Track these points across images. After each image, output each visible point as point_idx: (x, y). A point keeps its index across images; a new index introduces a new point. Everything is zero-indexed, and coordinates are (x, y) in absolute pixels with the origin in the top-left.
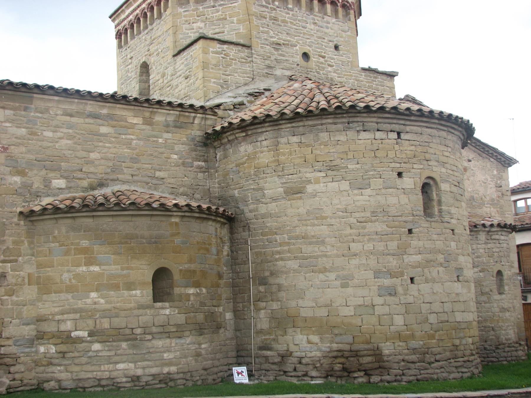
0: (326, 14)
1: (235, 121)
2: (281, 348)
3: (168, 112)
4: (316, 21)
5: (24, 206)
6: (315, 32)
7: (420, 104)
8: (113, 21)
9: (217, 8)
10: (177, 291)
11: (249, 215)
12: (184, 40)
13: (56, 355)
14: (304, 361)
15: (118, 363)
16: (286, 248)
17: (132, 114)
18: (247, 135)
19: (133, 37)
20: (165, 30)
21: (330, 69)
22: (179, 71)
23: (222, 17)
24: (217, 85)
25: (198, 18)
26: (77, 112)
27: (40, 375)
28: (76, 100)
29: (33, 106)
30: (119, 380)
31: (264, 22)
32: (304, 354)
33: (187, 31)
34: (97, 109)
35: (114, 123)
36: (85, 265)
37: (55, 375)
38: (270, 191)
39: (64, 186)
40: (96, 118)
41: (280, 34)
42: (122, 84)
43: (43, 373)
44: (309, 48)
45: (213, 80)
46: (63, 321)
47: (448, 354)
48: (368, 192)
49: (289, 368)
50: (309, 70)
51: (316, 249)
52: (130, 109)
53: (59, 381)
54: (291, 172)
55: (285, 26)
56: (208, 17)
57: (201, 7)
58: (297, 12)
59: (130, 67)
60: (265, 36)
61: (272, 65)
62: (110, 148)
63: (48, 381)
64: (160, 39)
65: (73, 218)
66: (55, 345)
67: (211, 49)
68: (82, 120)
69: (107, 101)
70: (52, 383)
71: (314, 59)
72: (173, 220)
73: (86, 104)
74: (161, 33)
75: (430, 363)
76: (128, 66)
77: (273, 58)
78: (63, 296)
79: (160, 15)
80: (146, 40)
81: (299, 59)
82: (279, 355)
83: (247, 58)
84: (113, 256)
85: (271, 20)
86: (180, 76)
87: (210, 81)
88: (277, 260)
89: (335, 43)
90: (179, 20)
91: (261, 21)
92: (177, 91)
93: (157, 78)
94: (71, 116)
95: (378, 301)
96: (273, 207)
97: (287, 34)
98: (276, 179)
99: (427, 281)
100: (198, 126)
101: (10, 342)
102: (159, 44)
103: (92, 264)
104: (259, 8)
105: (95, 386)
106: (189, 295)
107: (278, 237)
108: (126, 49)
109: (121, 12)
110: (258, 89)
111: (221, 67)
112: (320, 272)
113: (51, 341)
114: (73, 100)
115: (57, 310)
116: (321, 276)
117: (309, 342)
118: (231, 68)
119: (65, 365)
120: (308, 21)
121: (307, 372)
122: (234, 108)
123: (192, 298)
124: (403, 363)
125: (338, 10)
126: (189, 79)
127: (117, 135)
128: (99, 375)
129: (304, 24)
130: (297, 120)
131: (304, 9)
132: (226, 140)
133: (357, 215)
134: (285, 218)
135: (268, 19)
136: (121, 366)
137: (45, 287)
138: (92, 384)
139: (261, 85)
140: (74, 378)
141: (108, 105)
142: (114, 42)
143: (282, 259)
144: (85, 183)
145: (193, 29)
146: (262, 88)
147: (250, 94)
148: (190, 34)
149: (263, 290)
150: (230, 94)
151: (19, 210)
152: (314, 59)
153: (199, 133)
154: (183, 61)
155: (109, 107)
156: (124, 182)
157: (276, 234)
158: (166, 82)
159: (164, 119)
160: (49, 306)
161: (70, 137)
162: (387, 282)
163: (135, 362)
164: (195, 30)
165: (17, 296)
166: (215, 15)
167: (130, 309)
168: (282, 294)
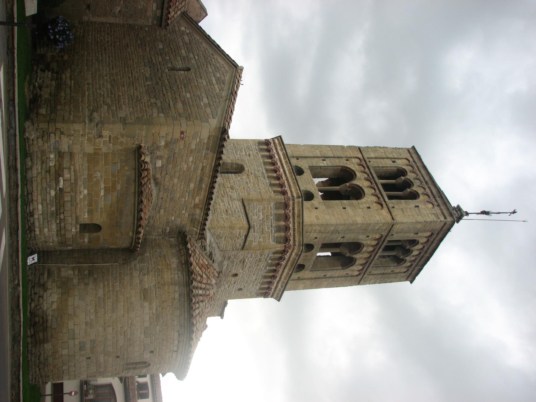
0: (262, 284)
1: (192, 259)
2: (49, 284)
5: (145, 147)
10: (87, 235)
11: (133, 263)
13: (48, 166)
14: (41, 299)
15: (42, 205)
16: (111, 289)
17: (201, 198)
18: (182, 264)
19: (263, 156)
21: (227, 286)
27: (35, 155)
29: (209, 152)
30: (31, 205)
32: (45, 299)
35: (196, 190)
36: (105, 187)
37: (35, 166)
38: (146, 279)
39: (157, 166)
42: (234, 144)
43: (37, 156)
46: (70, 171)
47: (44, 374)
48: (143, 336)
49: (37, 290)
51: (109, 308)
53: (31, 168)
54: (157, 293)
60: (249, 256)
62: (180, 188)
63: (31, 160)
66: (55, 166)
70: (30, 163)
71: (233, 279)
72: (131, 234)
74: (260, 187)
75: (38, 366)
77: (235, 259)
78: (86, 172)
79: (272, 185)
81: (234, 272)
82: (45, 283)
84: (110, 203)
88: (104, 282)
92: (220, 201)
93: (231, 182)
94: (202, 170)
95: (77, 342)
96: (137, 281)
98: (153, 284)
99: (88, 365)
100: (192, 230)
101: (57, 139)
103: (105, 191)
105: (28, 191)
106: (84, 239)
107: (118, 284)
112: (96, 310)
113: (57, 163)
115: (77, 168)
116: (93, 310)
117: (53, 302)
119: (41, 173)
121: (34, 301)
123: (82, 240)
124: (38, 354)
127: (188, 190)
128: (35, 194)
129: (256, 274)
131: (266, 274)
132: (181, 248)
133: (129, 331)
136: (40, 207)
137: (93, 159)
138: (29, 190)
139: (218, 256)
140: (33, 179)
141: (208, 189)
143: (104, 286)
144: (158, 176)
147: (211, 254)
149: (85, 273)
150: (212, 240)
151: (143, 145)
153: (187, 229)
156: (158, 195)
157: (120, 283)
160: (80, 162)
161: (188, 168)
162: (88, 346)
163: (42, 214)
165: (87, 143)
167: (76, 212)
168: (82, 286)
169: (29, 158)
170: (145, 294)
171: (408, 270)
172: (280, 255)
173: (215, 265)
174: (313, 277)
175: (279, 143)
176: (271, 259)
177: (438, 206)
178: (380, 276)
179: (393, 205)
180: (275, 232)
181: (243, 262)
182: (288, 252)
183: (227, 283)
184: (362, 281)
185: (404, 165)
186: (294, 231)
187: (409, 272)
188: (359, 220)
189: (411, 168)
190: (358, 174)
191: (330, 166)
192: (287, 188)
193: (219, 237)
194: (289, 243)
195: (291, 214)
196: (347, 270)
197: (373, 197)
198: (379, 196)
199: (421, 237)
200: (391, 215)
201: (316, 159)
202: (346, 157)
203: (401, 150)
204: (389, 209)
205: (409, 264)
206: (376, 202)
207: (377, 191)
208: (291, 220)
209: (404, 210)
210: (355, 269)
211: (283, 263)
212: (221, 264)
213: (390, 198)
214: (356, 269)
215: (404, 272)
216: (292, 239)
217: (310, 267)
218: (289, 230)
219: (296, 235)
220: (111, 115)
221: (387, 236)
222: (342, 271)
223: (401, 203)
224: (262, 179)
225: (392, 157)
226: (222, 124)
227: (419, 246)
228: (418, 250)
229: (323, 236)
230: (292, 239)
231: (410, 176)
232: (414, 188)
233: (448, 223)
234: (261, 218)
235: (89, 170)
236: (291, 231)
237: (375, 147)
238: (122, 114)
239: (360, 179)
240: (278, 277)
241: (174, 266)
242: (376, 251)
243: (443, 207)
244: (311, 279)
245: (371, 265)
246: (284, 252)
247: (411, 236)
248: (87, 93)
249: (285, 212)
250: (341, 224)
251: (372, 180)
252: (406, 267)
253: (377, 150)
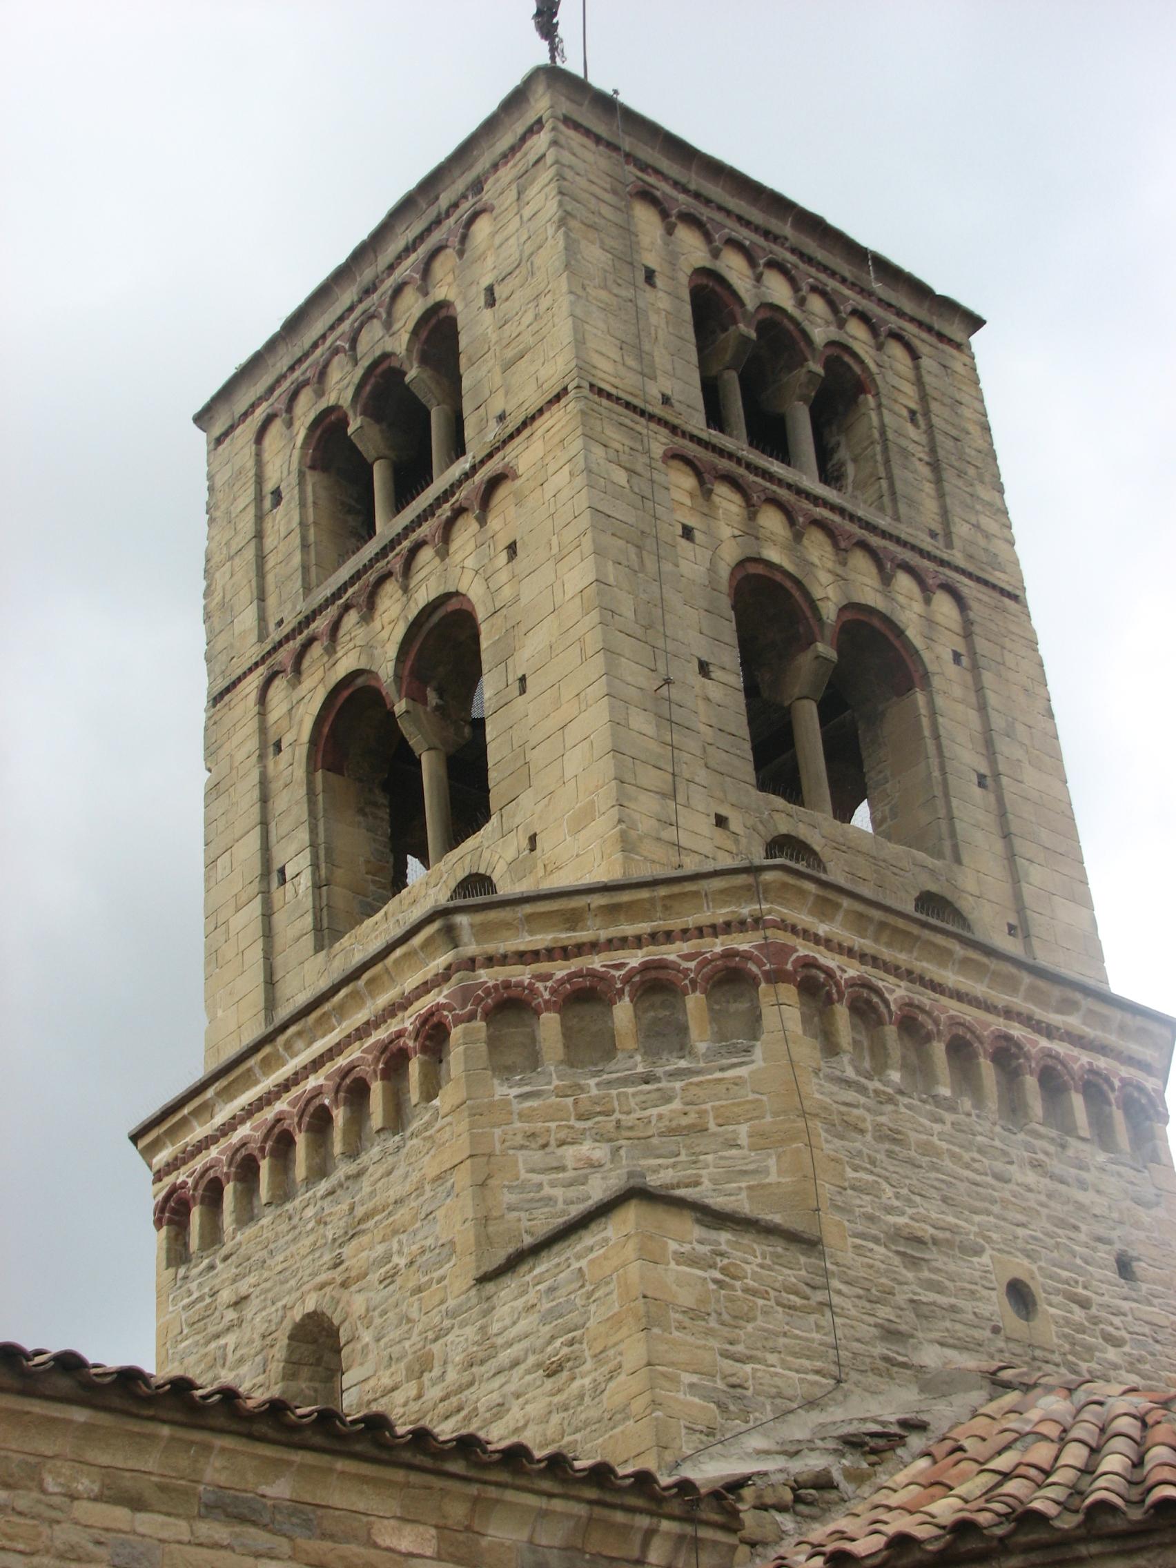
0: (1069, 1129)
3: (542, 1503)
4: (1041, 1156)
6: (1043, 1198)
8: (148, 1153)
9: (663, 1084)
12: (523, 1215)
19: (247, 1216)
20: (432, 1172)
21: (1112, 1354)
22: (509, 1344)
23: (685, 1121)
24: (704, 1397)
25: (580, 1125)
26: (162, 1488)
28: (166, 1431)
31: (858, 1145)
33: (536, 1178)
34: (250, 1476)
40: (242, 1519)
41: (918, 1199)
44: (1026, 1262)
45: (687, 1378)
50: (1038, 1353)
52: (391, 1484)
55: (934, 1168)
56: (628, 1120)
57: (592, 1082)
58: (969, 1115)
59: (230, 1340)
60: (864, 1203)
61: (903, 1328)
64: (402, 1214)
67: (673, 1246)
68: (183, 1524)
69: (296, 1438)
71: (1050, 1309)
73: (207, 1448)
74: (408, 1187)
76: (217, 1336)
77: (900, 1299)
79: (397, 1118)
80: (322, 1222)
81: (996, 1305)
83: (808, 1291)
85: (880, 1138)
86: (515, 1364)
87: (673, 1379)
89: (1118, 1246)
90: (498, 1132)
91: (846, 1143)
93: (386, 1381)
94: (137, 1504)
97: (945, 1200)
102: (395, 1232)
104: (835, 1088)
108: (212, 1267)
109: (195, 1113)
110: (875, 1421)
111: (713, 1324)
114: (150, 1427)
118: (750, 1327)
120: (1014, 1153)
122: (798, 1499)
125: (1110, 1116)
126: (565, 1375)
129: (999, 1166)
130: (1157, 1538)
131: (992, 1104)
135: (869, 1137)
139: (884, 1406)
141: (298, 1457)
142: (151, 1241)
145: (562, 1168)
146: (893, 1418)
147: (853, 1443)
148: (547, 1191)
152: (1052, 1310)
154: (531, 1297)
155: (302, 1466)
158: (434, 1393)
159: (523, 1535)
164: (570, 1174)
166: (654, 1111)
171: (897, 336)
172: (842, 1012)
173: (941, 1413)
174: (999, 846)
175: (173, 1133)
176: (879, 1070)
177: (477, 186)
178: (951, 481)
180: (683, 1047)
181: (911, 1246)
182: (809, 963)
183: (1090, 1349)
184: (998, 578)
185: (292, 438)
186: (669, 937)
187: (910, 329)
188: (578, 575)
189: (305, 397)
190: (346, 664)
191: (313, 831)
192: (407, 1021)
193: (733, 1399)
194: (747, 956)
195: (560, 970)
196: (926, 656)
197: (453, 547)
198: (446, 510)
199: (672, 259)
200: (541, 411)
201: (279, 919)
202: (262, 757)
203: (219, 481)
204: (511, 437)
205: (857, 333)
206: (482, 520)
207: (425, 530)
208: (596, 962)
209: (510, 353)
210: (907, 606)
211: (896, 992)
212: (937, 1385)
213: (458, 447)
214: (918, 607)
215: (915, 356)
216: (718, 946)
217: (930, 861)
218: (661, 965)
219: (691, 921)
221: (674, 429)
222: (936, 682)
224: (367, 1189)
225: (251, 511)
227: (734, 268)
228: (759, 278)
229: (702, 776)
230: (718, 946)
231: (342, 385)
232: (399, 343)
233: (565, 107)
234: (600, 1152)
236: (671, 953)
237: (208, 617)
239: (368, 648)
240: (998, 1024)
242: (783, 493)
244: (1011, 857)
245: (883, 522)
246: (814, 988)
247: (668, 311)
249: (549, 1006)
250: (610, 672)
251: (371, 576)
252: (880, 347)
253: (223, 605)
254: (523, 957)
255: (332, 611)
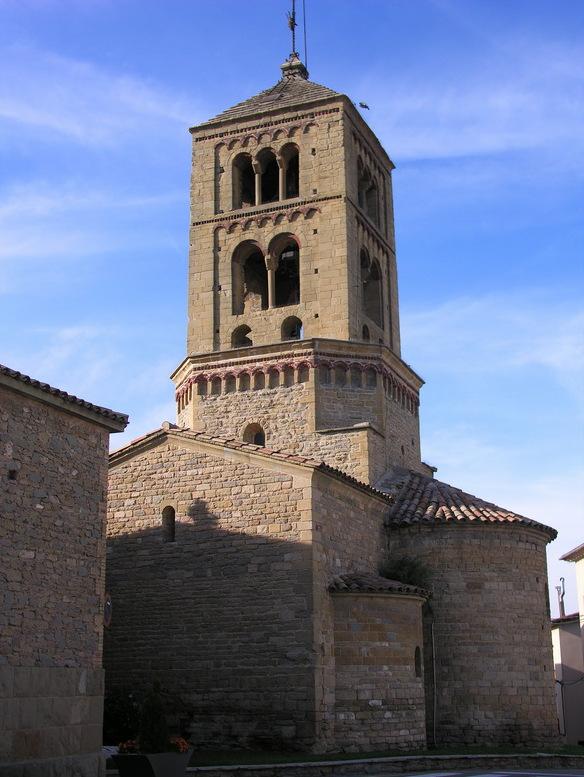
2: (463, 722)
7: (521, 517)
18: (433, 531)
36: (380, 640)
63: (348, 746)
65: (385, 598)
78: (363, 668)
79: (288, 383)
82: (460, 728)
95: (530, 684)
107: (460, 624)
117: (486, 717)
130: (155, 435)
134: (467, 609)
136: (402, 732)
143: (464, 644)
157: (459, 621)
169: (347, 749)
170: (475, 586)
177: (312, 115)
179: (311, 191)
190: (249, 236)
195: (337, 360)
220: (293, 631)
223: (306, 177)
226: (308, 469)
231: (253, 149)
232: (277, 146)
235: (359, 663)
236: (360, 361)
238: (288, 615)
241: (434, 544)
243: (317, 109)
248: (240, 667)
254: (329, 355)
255: (246, 218)
